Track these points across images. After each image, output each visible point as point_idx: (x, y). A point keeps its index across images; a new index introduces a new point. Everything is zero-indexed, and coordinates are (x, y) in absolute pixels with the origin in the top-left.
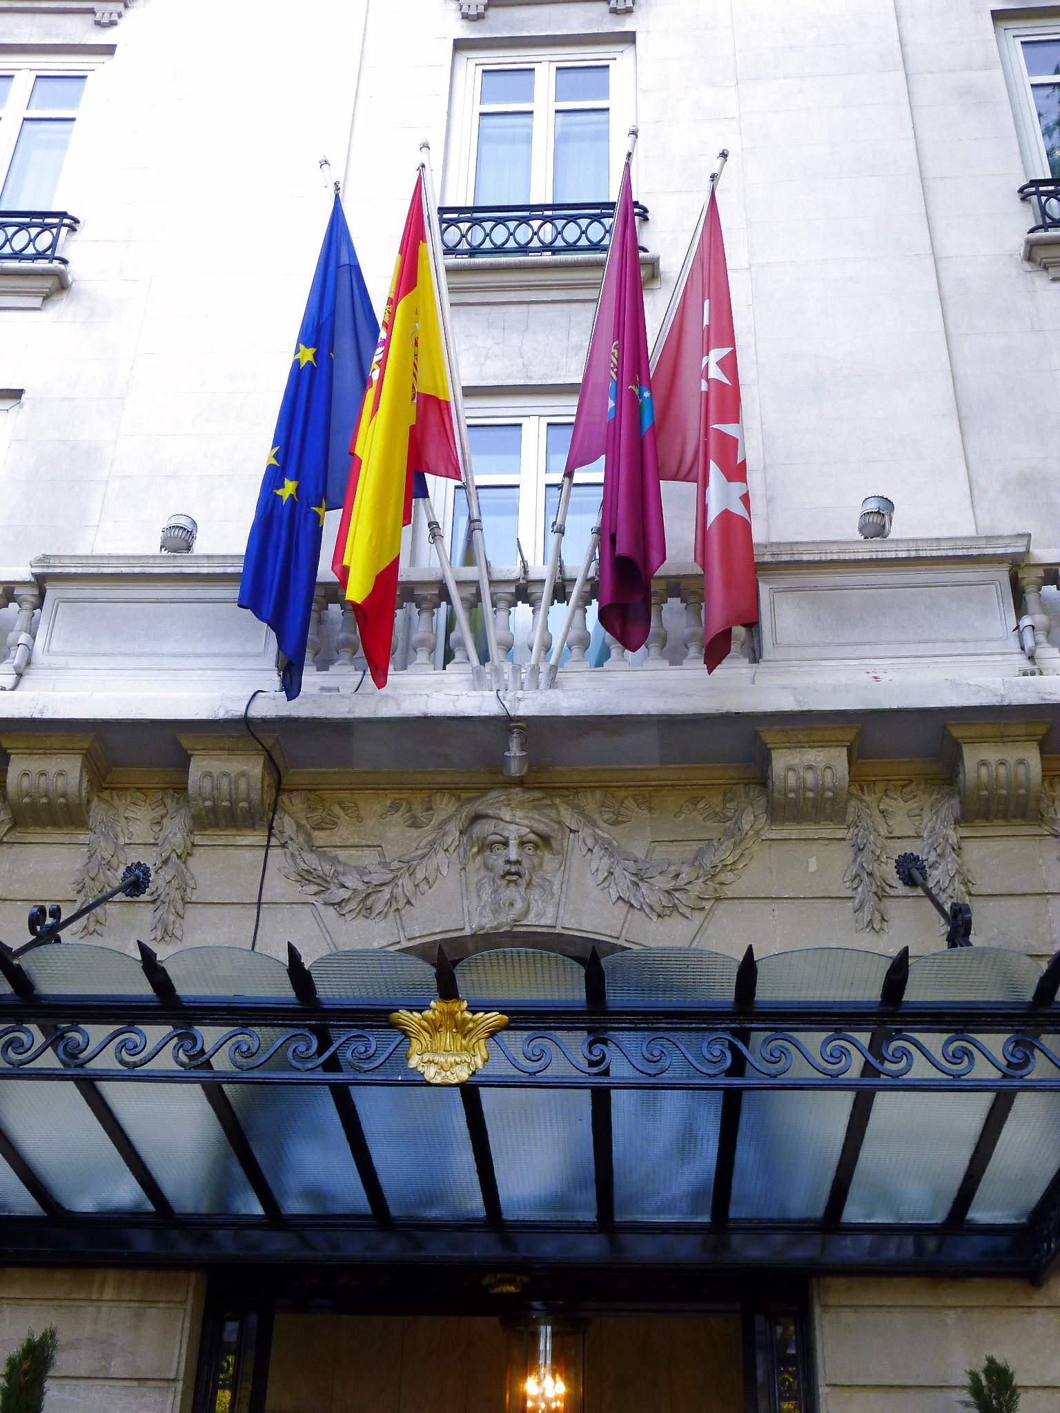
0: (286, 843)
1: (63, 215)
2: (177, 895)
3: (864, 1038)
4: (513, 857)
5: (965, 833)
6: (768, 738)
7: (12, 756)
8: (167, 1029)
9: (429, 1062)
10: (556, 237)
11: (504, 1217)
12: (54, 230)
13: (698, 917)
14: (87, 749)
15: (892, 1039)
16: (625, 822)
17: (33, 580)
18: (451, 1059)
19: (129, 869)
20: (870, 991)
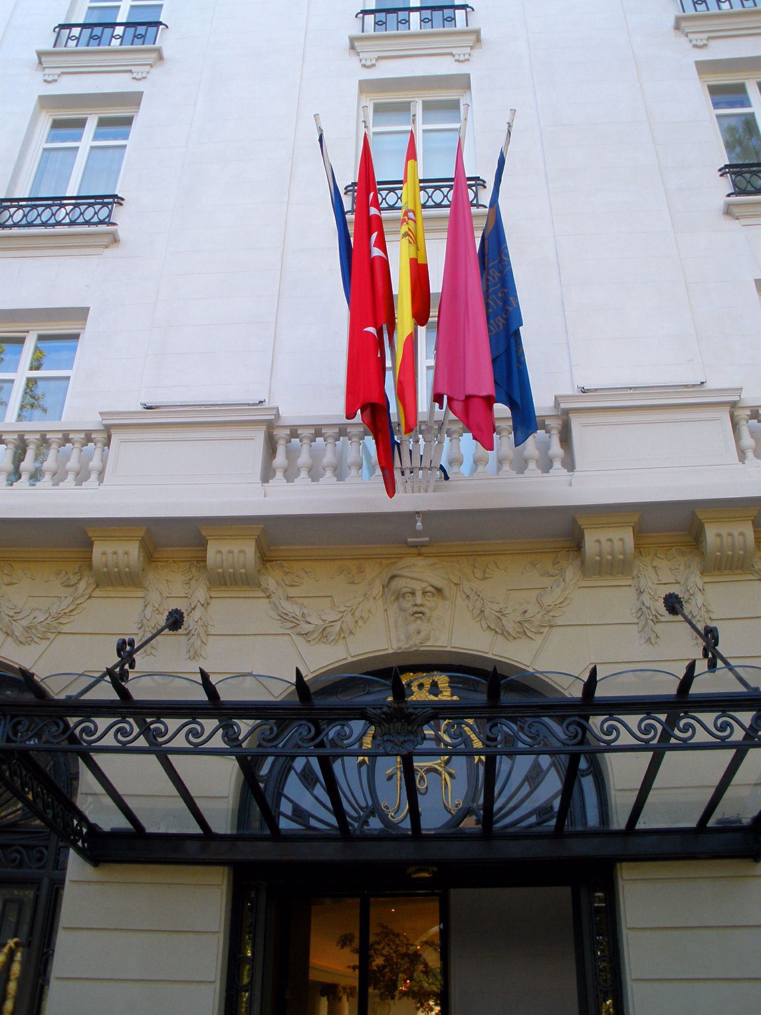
0: (271, 595)
2: (201, 630)
3: (663, 717)
4: (419, 601)
5: (707, 579)
6: (581, 522)
7: (95, 542)
8: (215, 723)
9: (388, 741)
10: (444, 199)
11: (147, 831)
12: (110, 206)
13: (539, 639)
14: (142, 537)
15: (683, 718)
17: (103, 428)
18: (402, 739)
19: (170, 613)
20: (672, 689)
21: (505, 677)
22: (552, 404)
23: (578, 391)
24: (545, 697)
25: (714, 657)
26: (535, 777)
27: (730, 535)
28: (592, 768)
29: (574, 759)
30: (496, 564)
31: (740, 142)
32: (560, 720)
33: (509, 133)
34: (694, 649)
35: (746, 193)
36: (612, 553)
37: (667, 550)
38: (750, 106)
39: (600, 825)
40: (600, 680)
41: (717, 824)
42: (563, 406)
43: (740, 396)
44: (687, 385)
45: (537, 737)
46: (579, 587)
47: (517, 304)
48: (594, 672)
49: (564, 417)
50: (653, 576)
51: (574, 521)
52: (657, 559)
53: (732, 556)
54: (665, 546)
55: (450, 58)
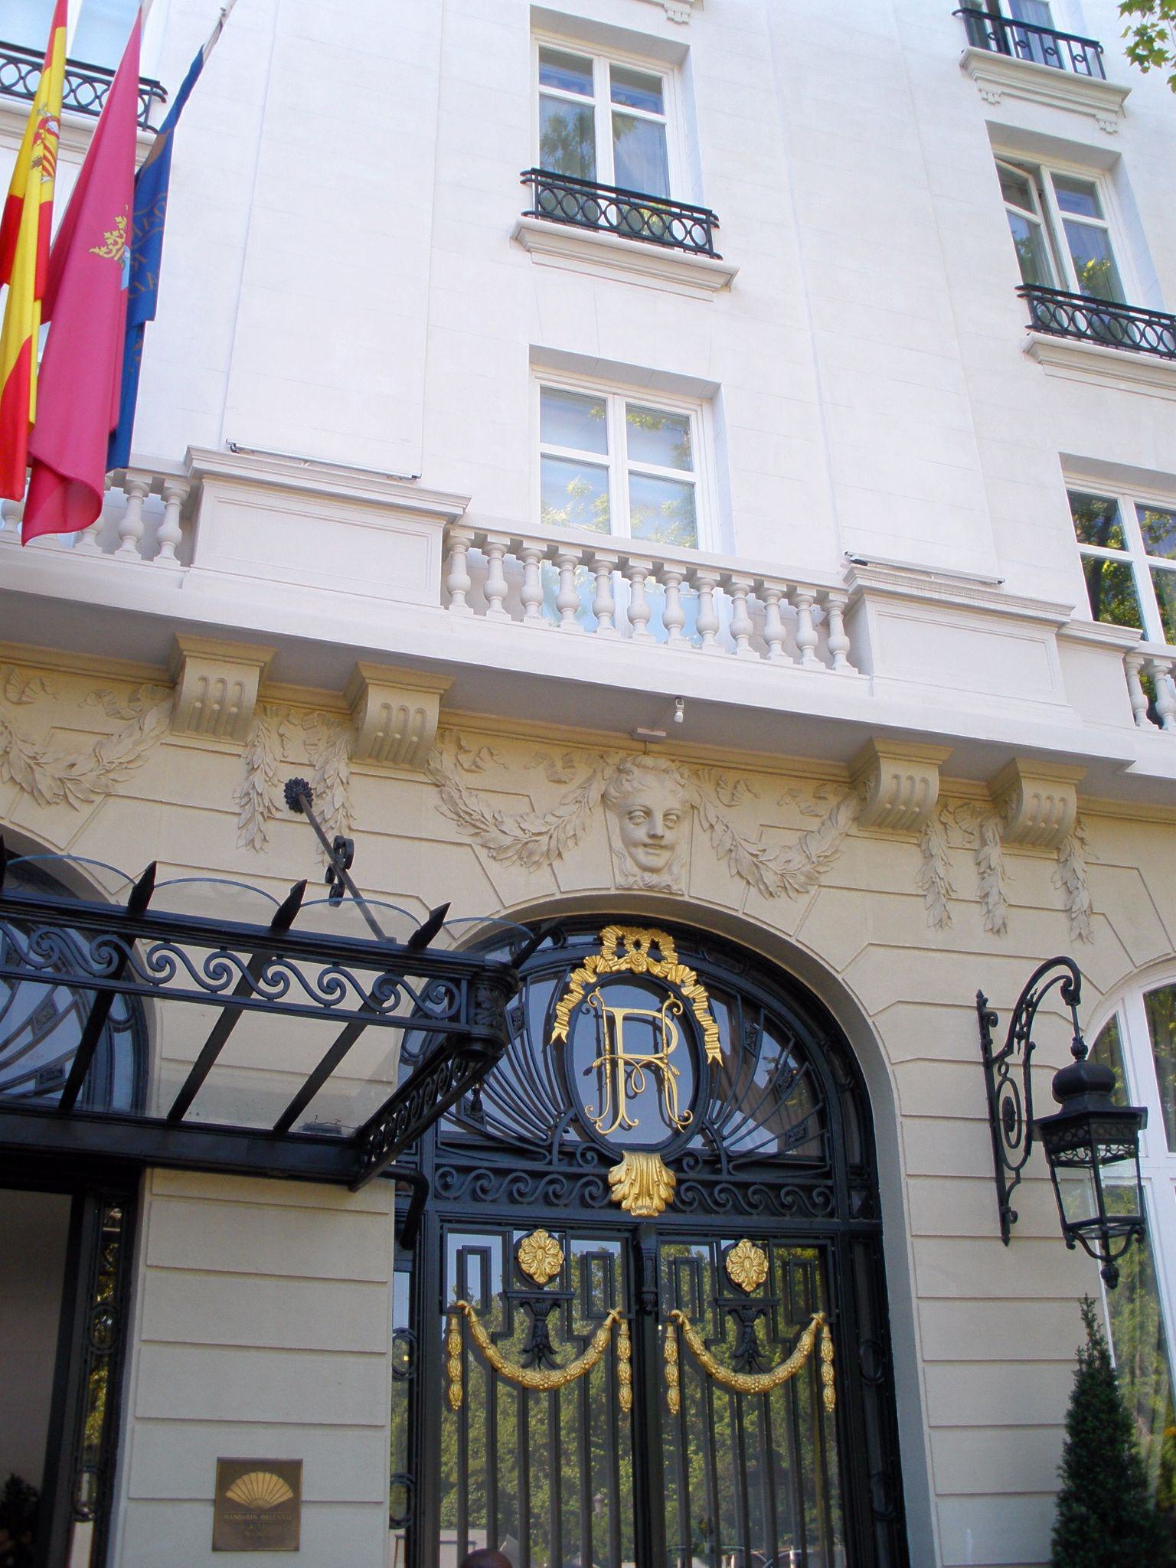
1: (708, 213)
3: (245, 958)
13: (86, 810)
15: (273, 963)
16: (28, 703)
20: (264, 918)
21: (14, 855)
22: (182, 459)
23: (227, 447)
24: (77, 897)
25: (341, 884)
26: (44, 1020)
27: (403, 709)
28: (133, 1021)
29: (104, 999)
30: (43, 684)
31: (565, 143)
32: (90, 934)
33: (221, 25)
34: (313, 867)
35: (551, 218)
36: (221, 702)
37: (306, 714)
38: (592, 95)
39: (131, 1107)
40: (158, 886)
41: (305, 1130)
42: (196, 464)
43: (464, 509)
44: (392, 476)
45: (51, 953)
46: (162, 744)
47: (156, 285)
48: (151, 872)
49: (196, 482)
50: (278, 750)
51: (174, 642)
52: (288, 724)
53: (401, 741)
54: (304, 708)
55: (1090, 121)
